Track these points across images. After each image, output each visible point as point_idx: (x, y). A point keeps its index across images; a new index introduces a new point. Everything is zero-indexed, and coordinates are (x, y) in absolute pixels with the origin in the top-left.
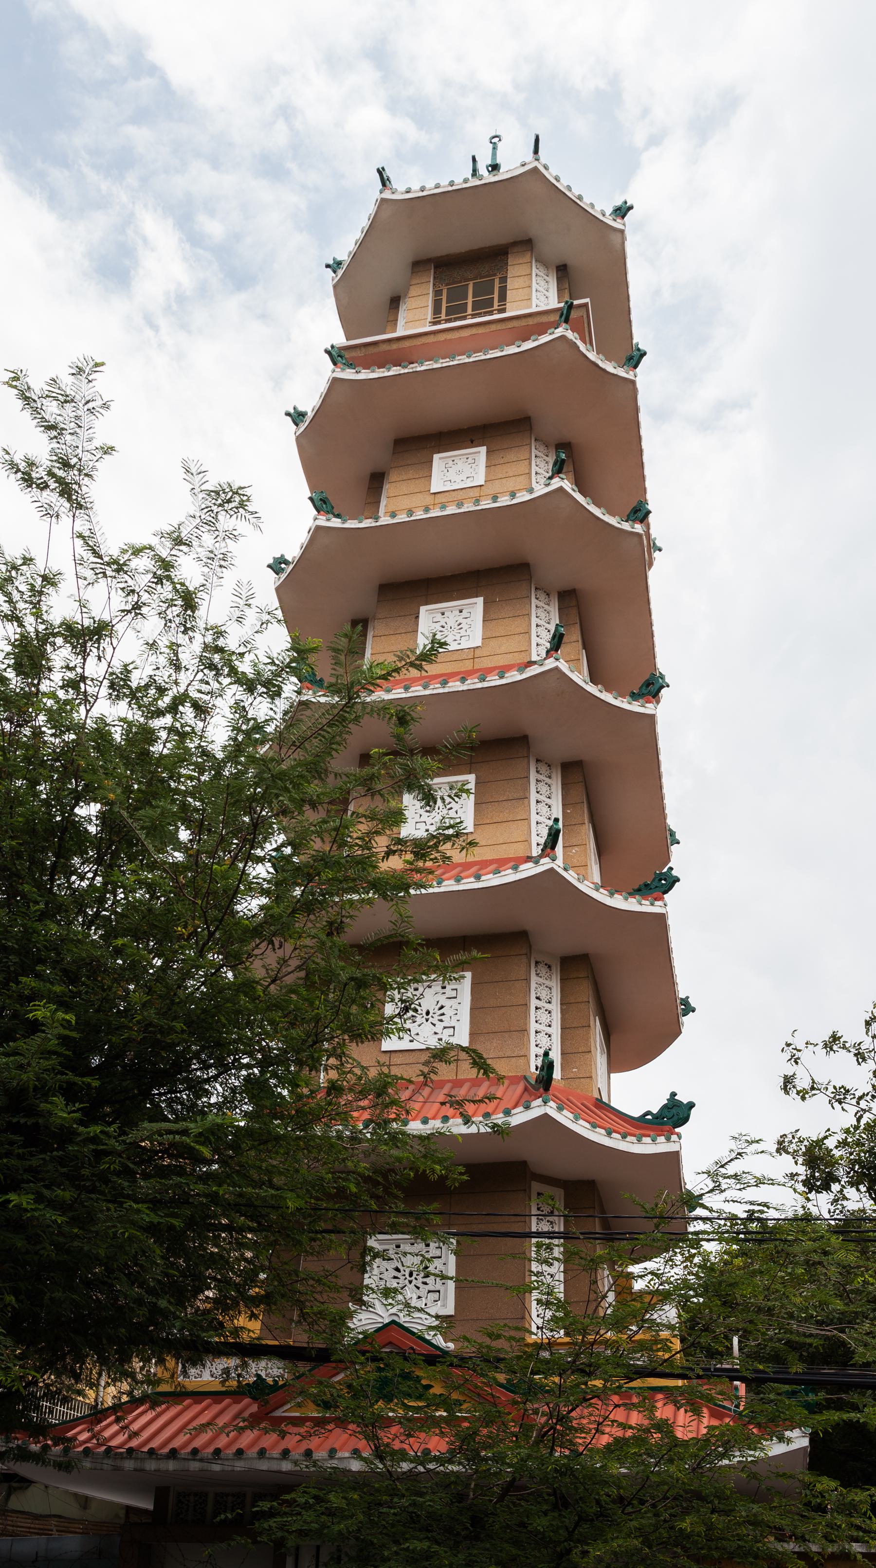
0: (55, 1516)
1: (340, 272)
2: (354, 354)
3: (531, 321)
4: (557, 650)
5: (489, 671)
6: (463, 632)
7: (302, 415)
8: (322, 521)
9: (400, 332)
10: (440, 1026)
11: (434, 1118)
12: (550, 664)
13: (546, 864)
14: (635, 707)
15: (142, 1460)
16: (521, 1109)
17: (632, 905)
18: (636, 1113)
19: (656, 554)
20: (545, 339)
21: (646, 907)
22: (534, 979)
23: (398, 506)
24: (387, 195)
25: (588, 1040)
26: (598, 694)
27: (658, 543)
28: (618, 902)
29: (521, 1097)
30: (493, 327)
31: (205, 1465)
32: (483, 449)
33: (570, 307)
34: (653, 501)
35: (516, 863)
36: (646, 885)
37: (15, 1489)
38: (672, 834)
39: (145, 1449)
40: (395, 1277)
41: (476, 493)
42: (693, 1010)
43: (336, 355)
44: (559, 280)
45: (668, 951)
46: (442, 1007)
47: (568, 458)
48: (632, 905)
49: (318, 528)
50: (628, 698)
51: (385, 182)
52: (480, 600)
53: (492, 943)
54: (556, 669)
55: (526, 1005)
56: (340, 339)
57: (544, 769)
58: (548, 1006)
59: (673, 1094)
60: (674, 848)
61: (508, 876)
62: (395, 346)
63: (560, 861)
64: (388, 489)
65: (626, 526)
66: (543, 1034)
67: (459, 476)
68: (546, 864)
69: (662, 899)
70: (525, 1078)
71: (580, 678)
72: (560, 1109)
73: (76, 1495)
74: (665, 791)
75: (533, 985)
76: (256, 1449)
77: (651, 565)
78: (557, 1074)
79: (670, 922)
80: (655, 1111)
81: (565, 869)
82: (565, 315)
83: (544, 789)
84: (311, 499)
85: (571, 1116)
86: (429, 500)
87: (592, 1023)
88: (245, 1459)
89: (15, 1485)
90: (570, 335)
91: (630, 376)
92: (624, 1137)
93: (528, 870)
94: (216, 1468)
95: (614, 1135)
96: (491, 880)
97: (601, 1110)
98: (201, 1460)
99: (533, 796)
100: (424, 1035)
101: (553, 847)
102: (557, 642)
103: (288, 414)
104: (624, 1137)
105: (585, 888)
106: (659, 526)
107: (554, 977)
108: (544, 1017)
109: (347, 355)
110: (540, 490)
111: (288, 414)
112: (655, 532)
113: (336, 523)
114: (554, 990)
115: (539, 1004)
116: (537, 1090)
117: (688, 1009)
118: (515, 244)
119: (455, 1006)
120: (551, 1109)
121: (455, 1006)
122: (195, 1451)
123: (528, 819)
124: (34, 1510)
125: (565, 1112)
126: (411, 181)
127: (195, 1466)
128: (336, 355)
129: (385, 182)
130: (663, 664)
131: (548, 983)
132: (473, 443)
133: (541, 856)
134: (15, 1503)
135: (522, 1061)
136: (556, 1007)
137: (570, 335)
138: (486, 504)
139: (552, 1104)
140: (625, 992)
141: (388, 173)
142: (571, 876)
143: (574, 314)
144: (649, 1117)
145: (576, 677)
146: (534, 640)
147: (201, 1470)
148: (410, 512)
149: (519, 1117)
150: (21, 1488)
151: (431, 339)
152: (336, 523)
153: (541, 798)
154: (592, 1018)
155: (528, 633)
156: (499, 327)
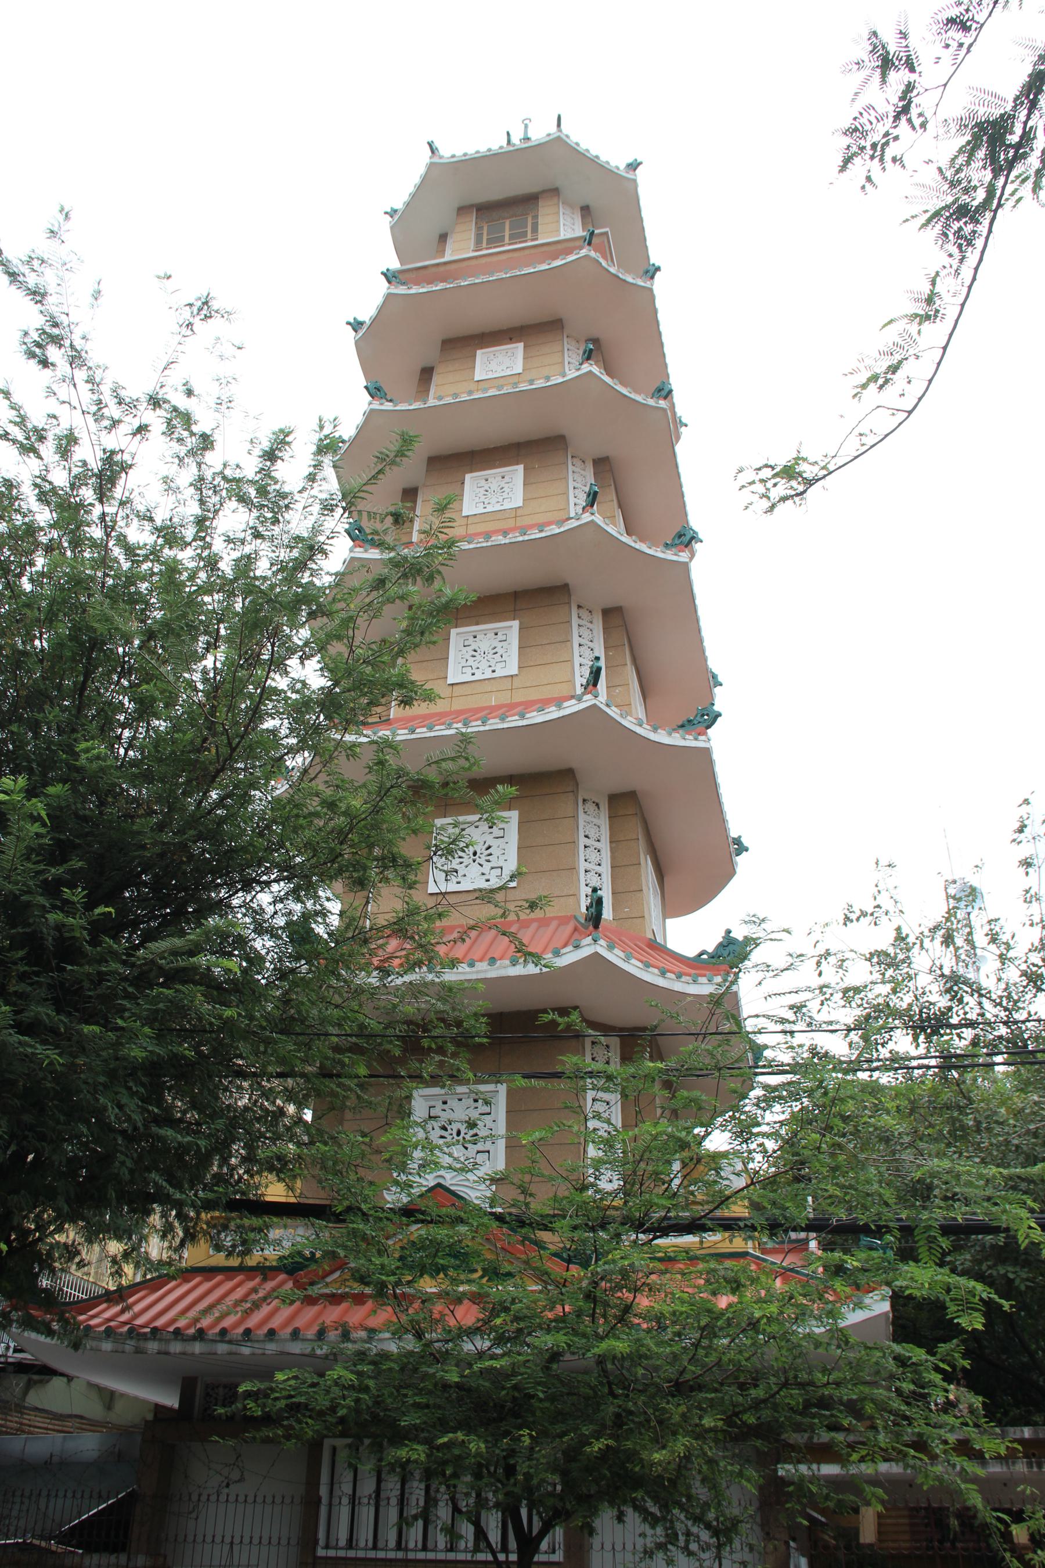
0: (76, 1416)
1: (396, 218)
2: (407, 275)
3: (559, 247)
4: (592, 506)
5: (531, 527)
6: (505, 495)
7: (361, 324)
8: (376, 405)
9: (447, 258)
10: (487, 866)
11: (481, 960)
12: (586, 518)
13: (588, 700)
14: (669, 555)
15: (168, 1341)
16: (570, 948)
17: (676, 739)
18: (691, 952)
19: (683, 429)
20: (571, 258)
21: (690, 742)
22: (582, 818)
23: (444, 392)
24: (436, 160)
25: (639, 878)
26: (633, 544)
27: (684, 420)
28: (662, 737)
29: (570, 937)
30: (527, 252)
31: (234, 1348)
32: (521, 345)
33: (592, 234)
34: (676, 382)
35: (559, 702)
36: (689, 721)
37: (36, 1382)
38: (714, 676)
39: (171, 1329)
40: (442, 1137)
41: (515, 379)
42: (747, 850)
43: (390, 276)
44: (583, 217)
45: (715, 786)
46: (489, 847)
47: (594, 350)
48: (676, 739)
49: (372, 411)
50: (662, 548)
51: (433, 150)
52: (520, 468)
53: (537, 783)
54: (592, 521)
55: (574, 843)
56: (395, 264)
57: (584, 613)
58: (597, 845)
59: (728, 932)
60: (717, 690)
61: (553, 713)
62: (442, 269)
63: (603, 697)
64: (436, 379)
65: (651, 402)
66: (593, 873)
67: (500, 366)
68: (588, 700)
69: (705, 734)
70: (575, 917)
71: (616, 530)
72: (610, 948)
73: (100, 1389)
74: (704, 633)
75: (581, 823)
76: (289, 1330)
77: (678, 438)
78: (607, 913)
79: (716, 756)
80: (710, 949)
81: (608, 705)
82: (589, 240)
83: (586, 633)
84: (366, 388)
85: (622, 954)
86: (473, 386)
87: (642, 861)
88: (277, 1341)
89: (35, 1377)
90: (593, 254)
91: (648, 285)
92: (679, 977)
93: (571, 707)
94: (246, 1351)
95: (669, 975)
96: (536, 717)
97: (656, 948)
98: (230, 1342)
99: (576, 640)
100: (472, 877)
101: (595, 685)
102: (592, 498)
103: (348, 323)
104: (679, 977)
105: (628, 723)
106: (683, 404)
107: (602, 815)
108: (594, 856)
109: (400, 276)
110: (572, 374)
111: (348, 323)
112: (680, 411)
113: (388, 406)
114: (603, 828)
115: (588, 842)
116: (587, 928)
117: (741, 848)
118: (544, 192)
119: (503, 846)
120: (601, 948)
121: (503, 846)
122: (224, 1332)
123: (571, 661)
124: (54, 1410)
125: (616, 951)
126: (452, 148)
127: (222, 1348)
128: (390, 276)
129: (433, 150)
130: (695, 522)
131: (596, 821)
132: (511, 340)
133: (584, 694)
134: (33, 1398)
135: (571, 900)
136: (605, 846)
137: (593, 254)
138: (524, 387)
139: (602, 942)
140: (671, 828)
141: (437, 144)
142: (613, 712)
143: (594, 240)
144: (705, 957)
145: (611, 529)
146: (572, 500)
147: (230, 1354)
148: (456, 395)
149: (569, 957)
150: (41, 1381)
151: (474, 262)
152: (388, 406)
153: (583, 642)
154: (642, 856)
155: (566, 494)
156: (532, 251)
